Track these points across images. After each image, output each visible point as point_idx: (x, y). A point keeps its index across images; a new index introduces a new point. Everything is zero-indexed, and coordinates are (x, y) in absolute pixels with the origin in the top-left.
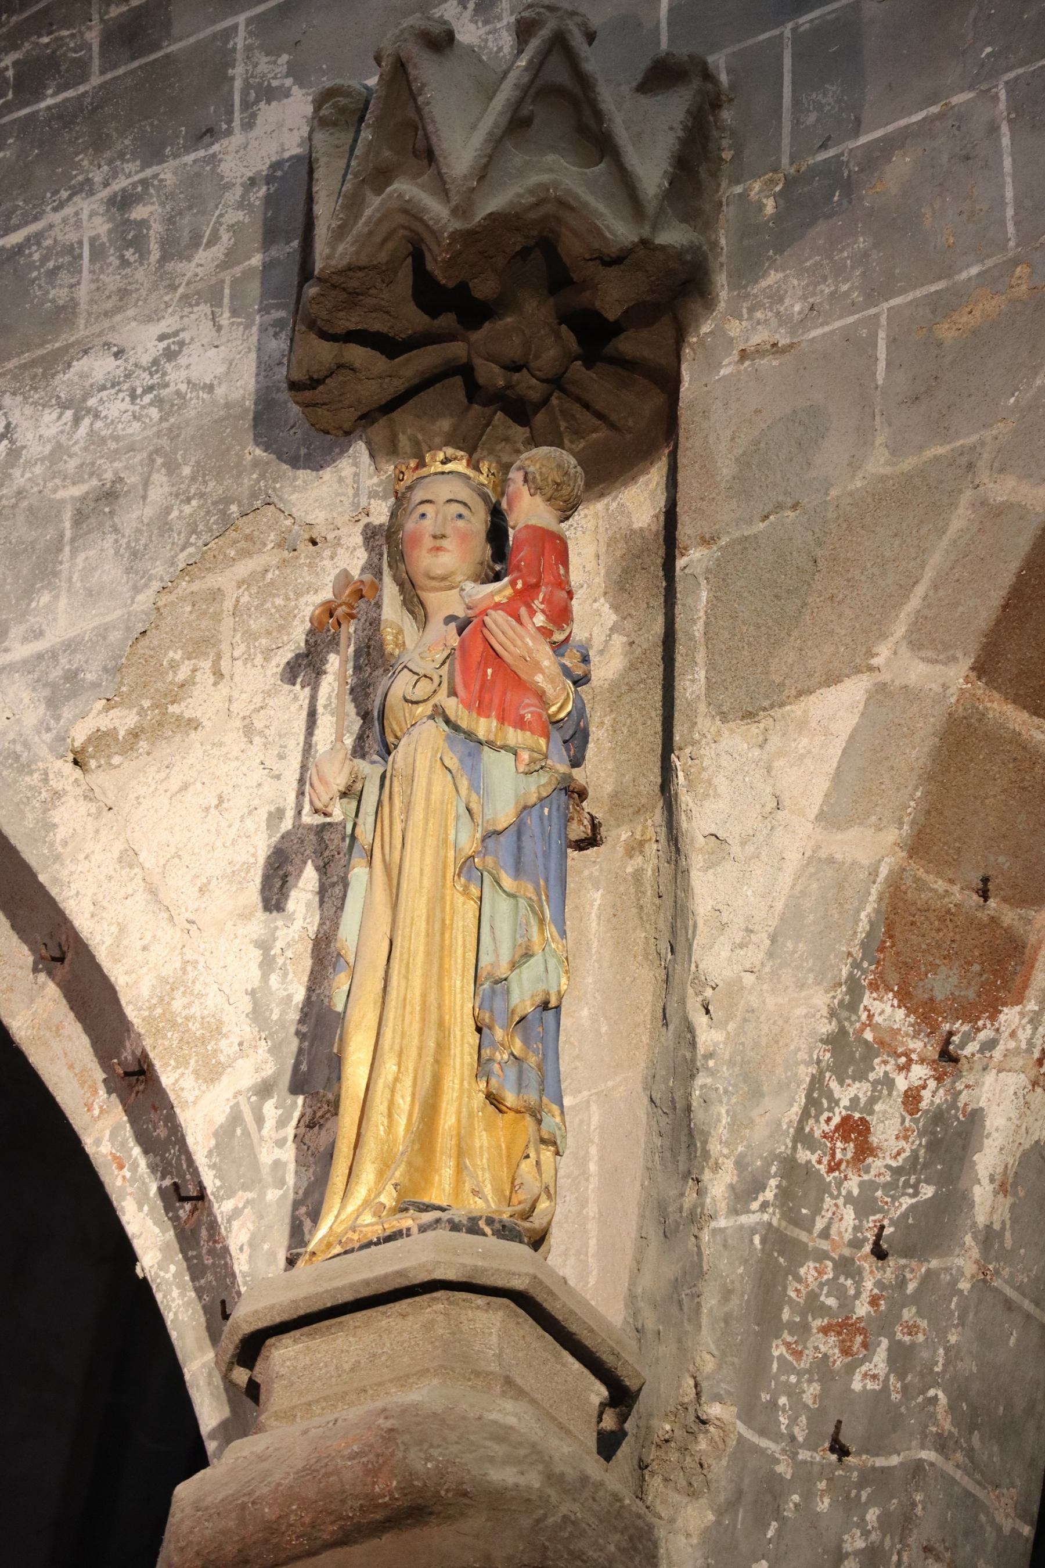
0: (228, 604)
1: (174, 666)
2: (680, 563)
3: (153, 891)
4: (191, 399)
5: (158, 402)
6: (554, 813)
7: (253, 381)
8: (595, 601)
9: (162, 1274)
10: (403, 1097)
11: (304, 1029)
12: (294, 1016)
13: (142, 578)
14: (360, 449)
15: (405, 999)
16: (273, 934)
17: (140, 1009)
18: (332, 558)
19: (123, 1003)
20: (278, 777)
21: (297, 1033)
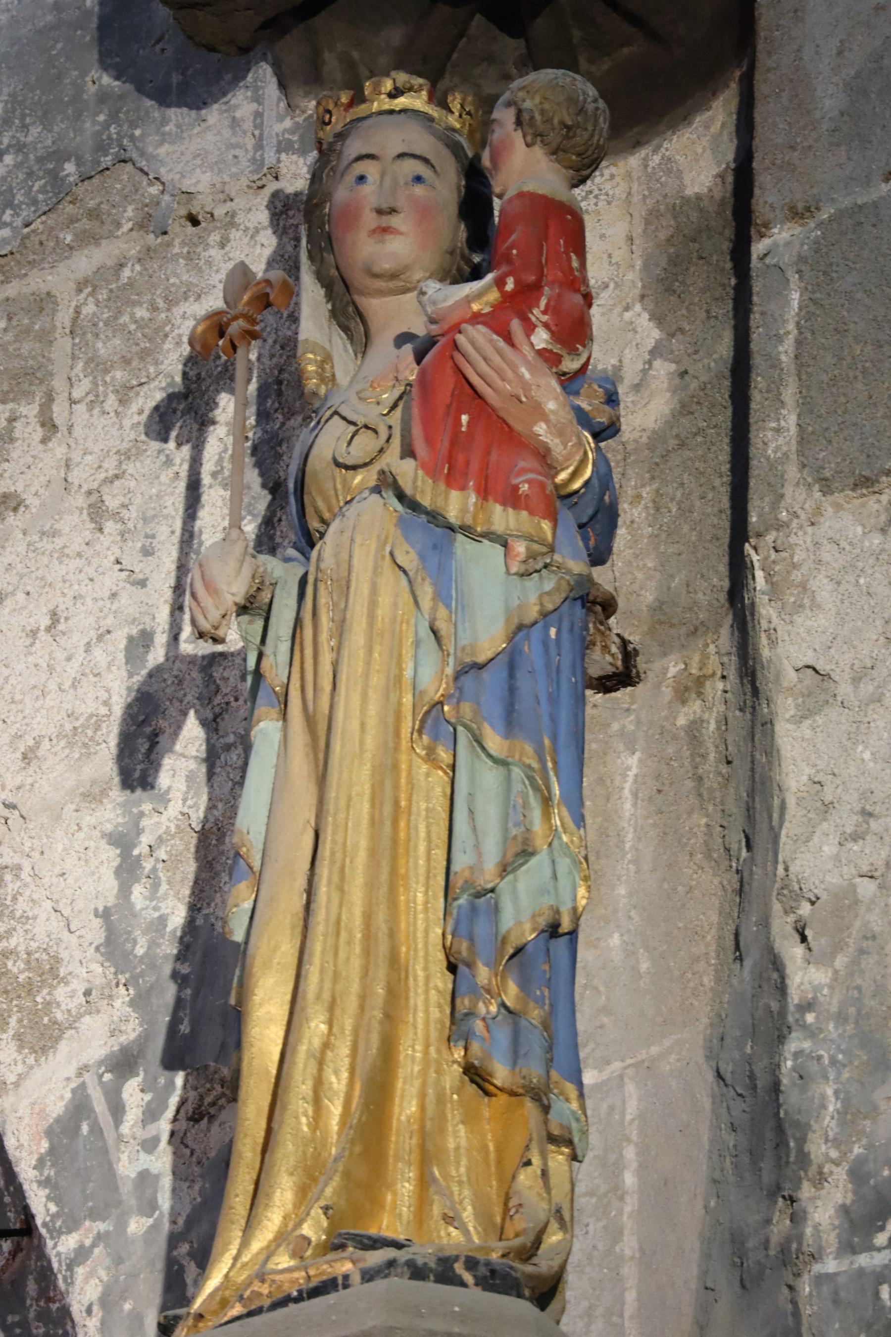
0: (64, 317)
2: (758, 248)
6: (565, 635)
8: (627, 308)
10: (336, 1072)
11: (185, 969)
12: (169, 948)
14: (264, 75)
15: (338, 922)
16: (137, 824)
18: (222, 245)
20: (143, 583)
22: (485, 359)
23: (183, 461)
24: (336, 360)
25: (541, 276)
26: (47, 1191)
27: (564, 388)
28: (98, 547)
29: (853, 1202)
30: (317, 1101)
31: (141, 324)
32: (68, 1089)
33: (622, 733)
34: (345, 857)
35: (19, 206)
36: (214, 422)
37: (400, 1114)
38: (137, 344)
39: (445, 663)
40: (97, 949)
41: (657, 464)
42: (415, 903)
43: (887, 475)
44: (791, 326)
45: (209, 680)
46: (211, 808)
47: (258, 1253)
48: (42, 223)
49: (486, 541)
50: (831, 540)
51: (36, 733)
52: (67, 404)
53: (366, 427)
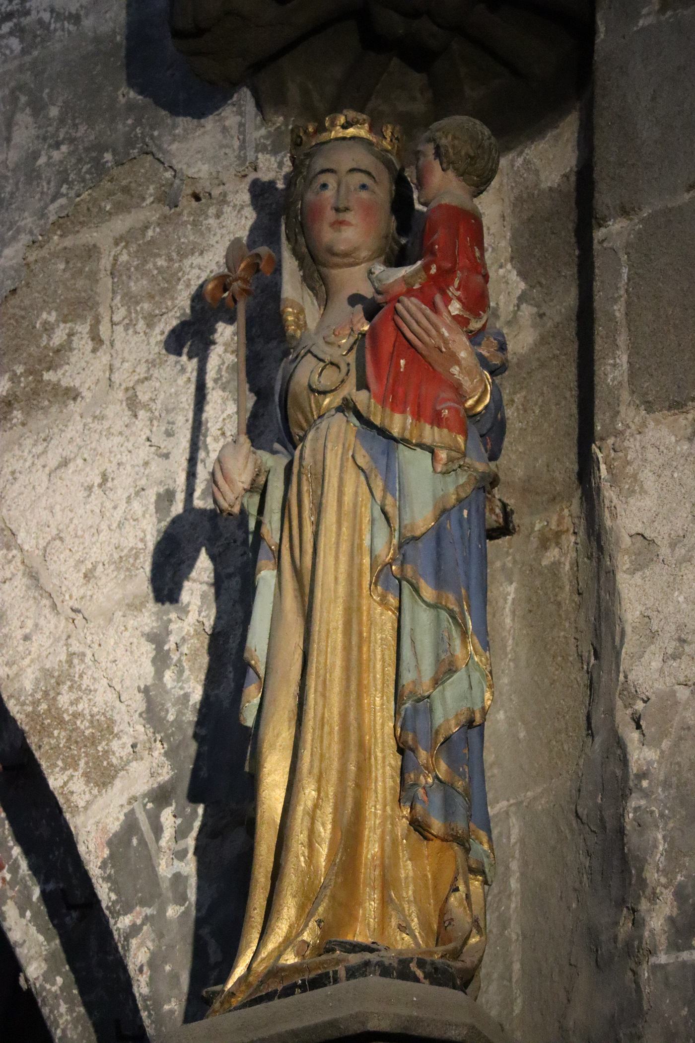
0: (106, 263)
1: (49, 329)
2: (599, 234)
3: (33, 576)
4: (55, 30)
6: (473, 513)
7: (123, 15)
8: (501, 267)
9: (48, 986)
10: (323, 825)
11: (203, 732)
12: (191, 717)
13: (9, 229)
14: (245, 97)
15: (323, 718)
16: (167, 628)
17: (23, 704)
18: (218, 216)
20: (167, 456)
21: (196, 736)
22: (417, 322)
23: (193, 370)
24: (306, 311)
25: (455, 263)
26: (109, 884)
27: (471, 341)
28: (134, 429)
29: (678, 915)
30: (311, 845)
31: (160, 270)
32: (122, 813)
35: (72, 182)
36: (214, 343)
37: (367, 854)
38: (159, 285)
40: (140, 715)
42: (375, 705)
43: (692, 401)
47: (272, 951)
48: (89, 195)
49: (418, 449)
50: (653, 445)
51: (93, 560)
52: (109, 325)
53: (332, 363)
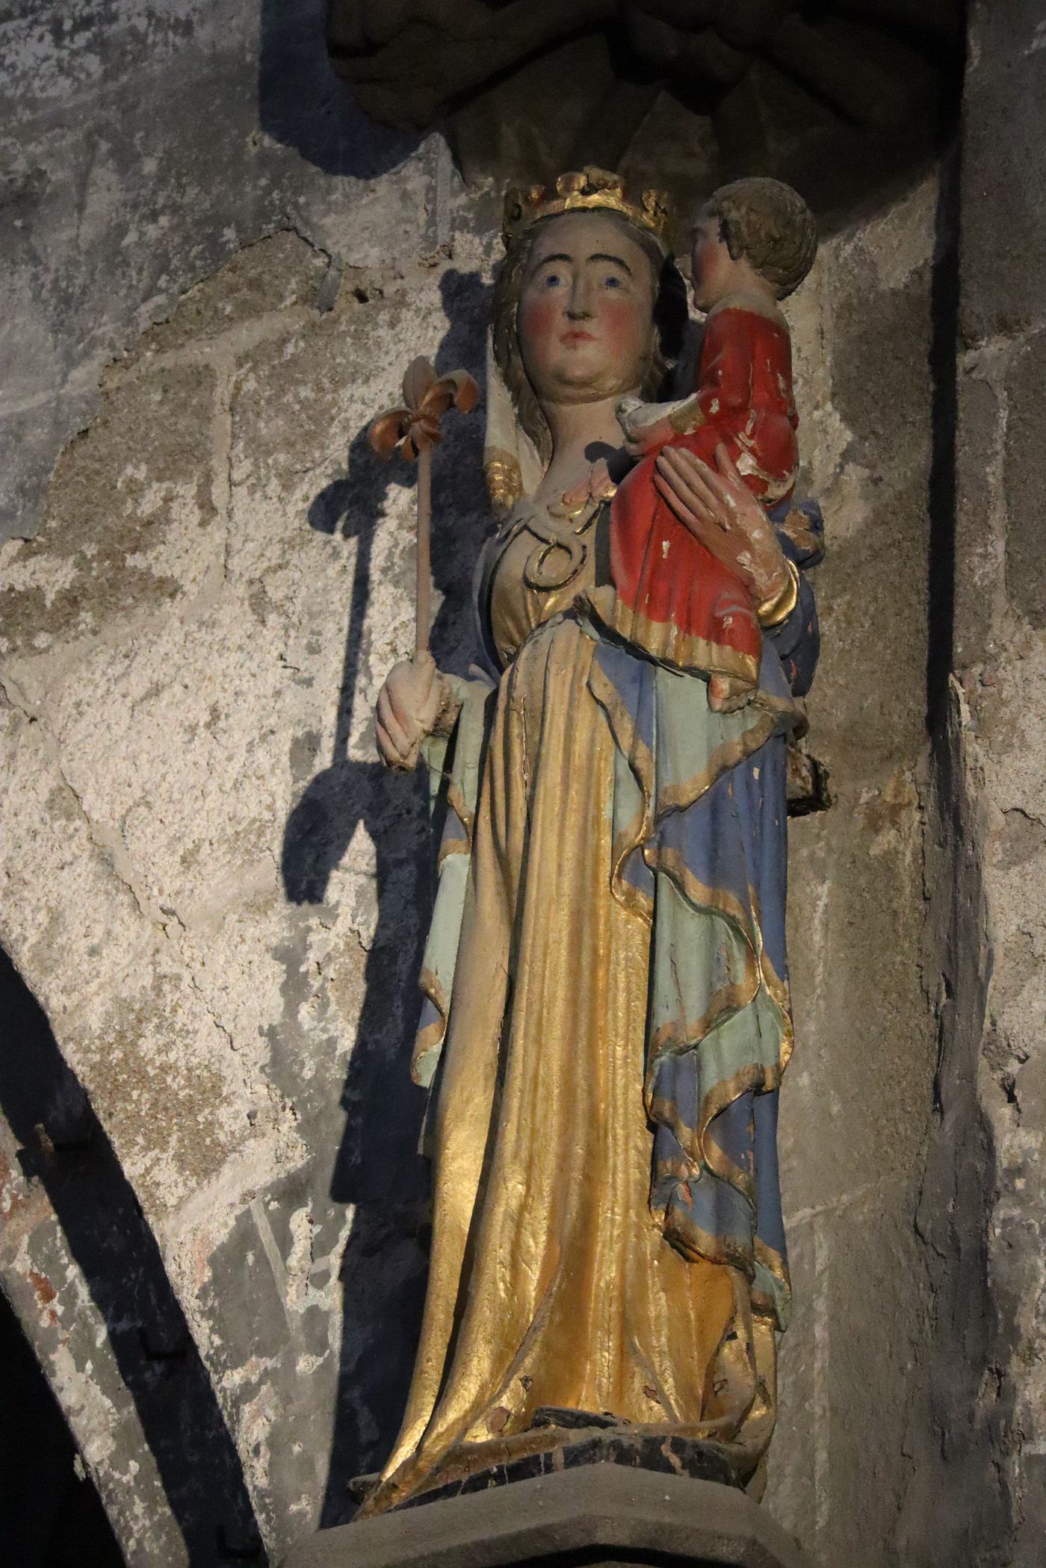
1: (135, 489)
2: (965, 359)
3: (105, 859)
4: (155, 44)
5: (99, 45)
6: (769, 776)
8: (816, 408)
9: (117, 1475)
10: (534, 1236)
11: (356, 1097)
12: (338, 1073)
14: (437, 145)
15: (536, 1077)
16: (304, 939)
17: (87, 1050)
18: (392, 325)
19: (59, 1039)
20: (308, 682)
21: (344, 1102)
22: (689, 485)
23: (350, 554)
24: (523, 466)
25: (748, 397)
26: (211, 1323)
28: (260, 641)
30: (514, 1266)
32: (233, 1216)
33: (812, 858)
34: (542, 1007)
35: (175, 271)
36: (382, 514)
37: (599, 1280)
38: (302, 426)
39: (644, 804)
40: (262, 1069)
41: (849, 575)
42: (614, 1057)
44: (999, 447)
45: (380, 790)
46: (381, 926)
49: (687, 676)
51: (195, 836)
53: (559, 546)
